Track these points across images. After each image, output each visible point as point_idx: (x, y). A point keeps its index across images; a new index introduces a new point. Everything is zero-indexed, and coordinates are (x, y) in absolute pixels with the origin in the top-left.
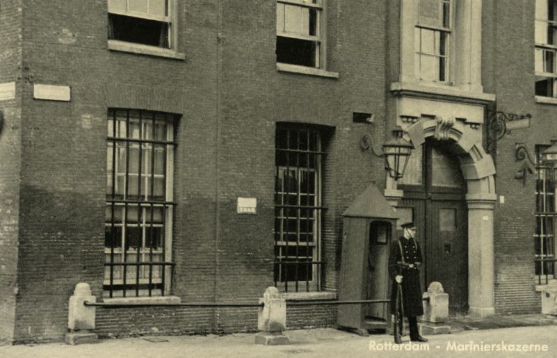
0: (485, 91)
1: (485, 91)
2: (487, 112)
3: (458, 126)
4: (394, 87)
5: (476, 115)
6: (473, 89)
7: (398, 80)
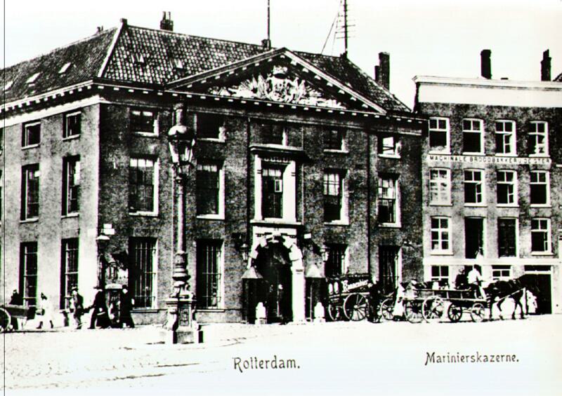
0: (297, 221)
1: (297, 221)
2: (298, 232)
3: (284, 237)
4: (252, 221)
5: (293, 232)
6: (293, 221)
7: (253, 218)
